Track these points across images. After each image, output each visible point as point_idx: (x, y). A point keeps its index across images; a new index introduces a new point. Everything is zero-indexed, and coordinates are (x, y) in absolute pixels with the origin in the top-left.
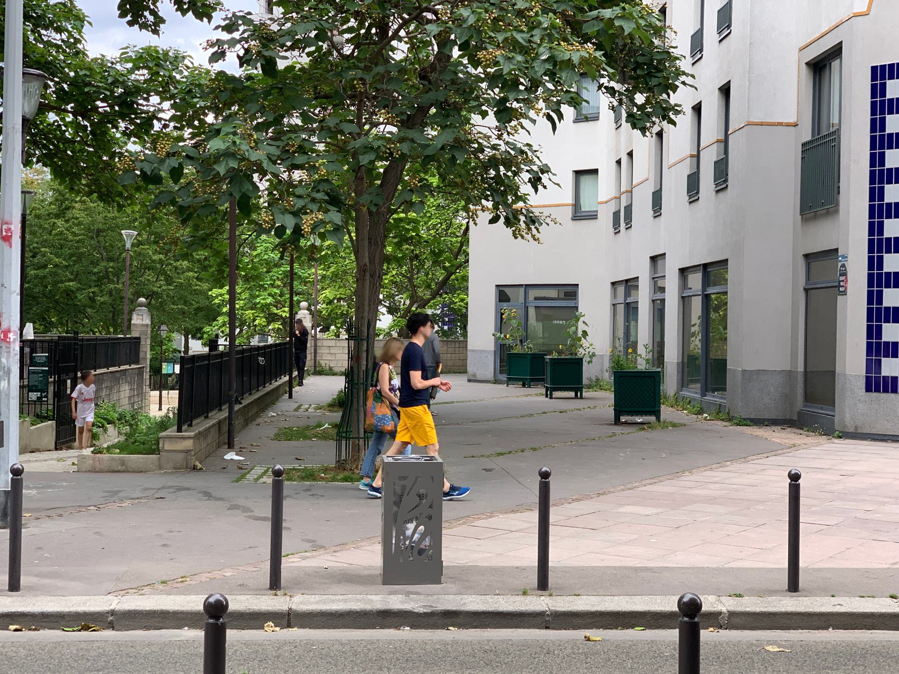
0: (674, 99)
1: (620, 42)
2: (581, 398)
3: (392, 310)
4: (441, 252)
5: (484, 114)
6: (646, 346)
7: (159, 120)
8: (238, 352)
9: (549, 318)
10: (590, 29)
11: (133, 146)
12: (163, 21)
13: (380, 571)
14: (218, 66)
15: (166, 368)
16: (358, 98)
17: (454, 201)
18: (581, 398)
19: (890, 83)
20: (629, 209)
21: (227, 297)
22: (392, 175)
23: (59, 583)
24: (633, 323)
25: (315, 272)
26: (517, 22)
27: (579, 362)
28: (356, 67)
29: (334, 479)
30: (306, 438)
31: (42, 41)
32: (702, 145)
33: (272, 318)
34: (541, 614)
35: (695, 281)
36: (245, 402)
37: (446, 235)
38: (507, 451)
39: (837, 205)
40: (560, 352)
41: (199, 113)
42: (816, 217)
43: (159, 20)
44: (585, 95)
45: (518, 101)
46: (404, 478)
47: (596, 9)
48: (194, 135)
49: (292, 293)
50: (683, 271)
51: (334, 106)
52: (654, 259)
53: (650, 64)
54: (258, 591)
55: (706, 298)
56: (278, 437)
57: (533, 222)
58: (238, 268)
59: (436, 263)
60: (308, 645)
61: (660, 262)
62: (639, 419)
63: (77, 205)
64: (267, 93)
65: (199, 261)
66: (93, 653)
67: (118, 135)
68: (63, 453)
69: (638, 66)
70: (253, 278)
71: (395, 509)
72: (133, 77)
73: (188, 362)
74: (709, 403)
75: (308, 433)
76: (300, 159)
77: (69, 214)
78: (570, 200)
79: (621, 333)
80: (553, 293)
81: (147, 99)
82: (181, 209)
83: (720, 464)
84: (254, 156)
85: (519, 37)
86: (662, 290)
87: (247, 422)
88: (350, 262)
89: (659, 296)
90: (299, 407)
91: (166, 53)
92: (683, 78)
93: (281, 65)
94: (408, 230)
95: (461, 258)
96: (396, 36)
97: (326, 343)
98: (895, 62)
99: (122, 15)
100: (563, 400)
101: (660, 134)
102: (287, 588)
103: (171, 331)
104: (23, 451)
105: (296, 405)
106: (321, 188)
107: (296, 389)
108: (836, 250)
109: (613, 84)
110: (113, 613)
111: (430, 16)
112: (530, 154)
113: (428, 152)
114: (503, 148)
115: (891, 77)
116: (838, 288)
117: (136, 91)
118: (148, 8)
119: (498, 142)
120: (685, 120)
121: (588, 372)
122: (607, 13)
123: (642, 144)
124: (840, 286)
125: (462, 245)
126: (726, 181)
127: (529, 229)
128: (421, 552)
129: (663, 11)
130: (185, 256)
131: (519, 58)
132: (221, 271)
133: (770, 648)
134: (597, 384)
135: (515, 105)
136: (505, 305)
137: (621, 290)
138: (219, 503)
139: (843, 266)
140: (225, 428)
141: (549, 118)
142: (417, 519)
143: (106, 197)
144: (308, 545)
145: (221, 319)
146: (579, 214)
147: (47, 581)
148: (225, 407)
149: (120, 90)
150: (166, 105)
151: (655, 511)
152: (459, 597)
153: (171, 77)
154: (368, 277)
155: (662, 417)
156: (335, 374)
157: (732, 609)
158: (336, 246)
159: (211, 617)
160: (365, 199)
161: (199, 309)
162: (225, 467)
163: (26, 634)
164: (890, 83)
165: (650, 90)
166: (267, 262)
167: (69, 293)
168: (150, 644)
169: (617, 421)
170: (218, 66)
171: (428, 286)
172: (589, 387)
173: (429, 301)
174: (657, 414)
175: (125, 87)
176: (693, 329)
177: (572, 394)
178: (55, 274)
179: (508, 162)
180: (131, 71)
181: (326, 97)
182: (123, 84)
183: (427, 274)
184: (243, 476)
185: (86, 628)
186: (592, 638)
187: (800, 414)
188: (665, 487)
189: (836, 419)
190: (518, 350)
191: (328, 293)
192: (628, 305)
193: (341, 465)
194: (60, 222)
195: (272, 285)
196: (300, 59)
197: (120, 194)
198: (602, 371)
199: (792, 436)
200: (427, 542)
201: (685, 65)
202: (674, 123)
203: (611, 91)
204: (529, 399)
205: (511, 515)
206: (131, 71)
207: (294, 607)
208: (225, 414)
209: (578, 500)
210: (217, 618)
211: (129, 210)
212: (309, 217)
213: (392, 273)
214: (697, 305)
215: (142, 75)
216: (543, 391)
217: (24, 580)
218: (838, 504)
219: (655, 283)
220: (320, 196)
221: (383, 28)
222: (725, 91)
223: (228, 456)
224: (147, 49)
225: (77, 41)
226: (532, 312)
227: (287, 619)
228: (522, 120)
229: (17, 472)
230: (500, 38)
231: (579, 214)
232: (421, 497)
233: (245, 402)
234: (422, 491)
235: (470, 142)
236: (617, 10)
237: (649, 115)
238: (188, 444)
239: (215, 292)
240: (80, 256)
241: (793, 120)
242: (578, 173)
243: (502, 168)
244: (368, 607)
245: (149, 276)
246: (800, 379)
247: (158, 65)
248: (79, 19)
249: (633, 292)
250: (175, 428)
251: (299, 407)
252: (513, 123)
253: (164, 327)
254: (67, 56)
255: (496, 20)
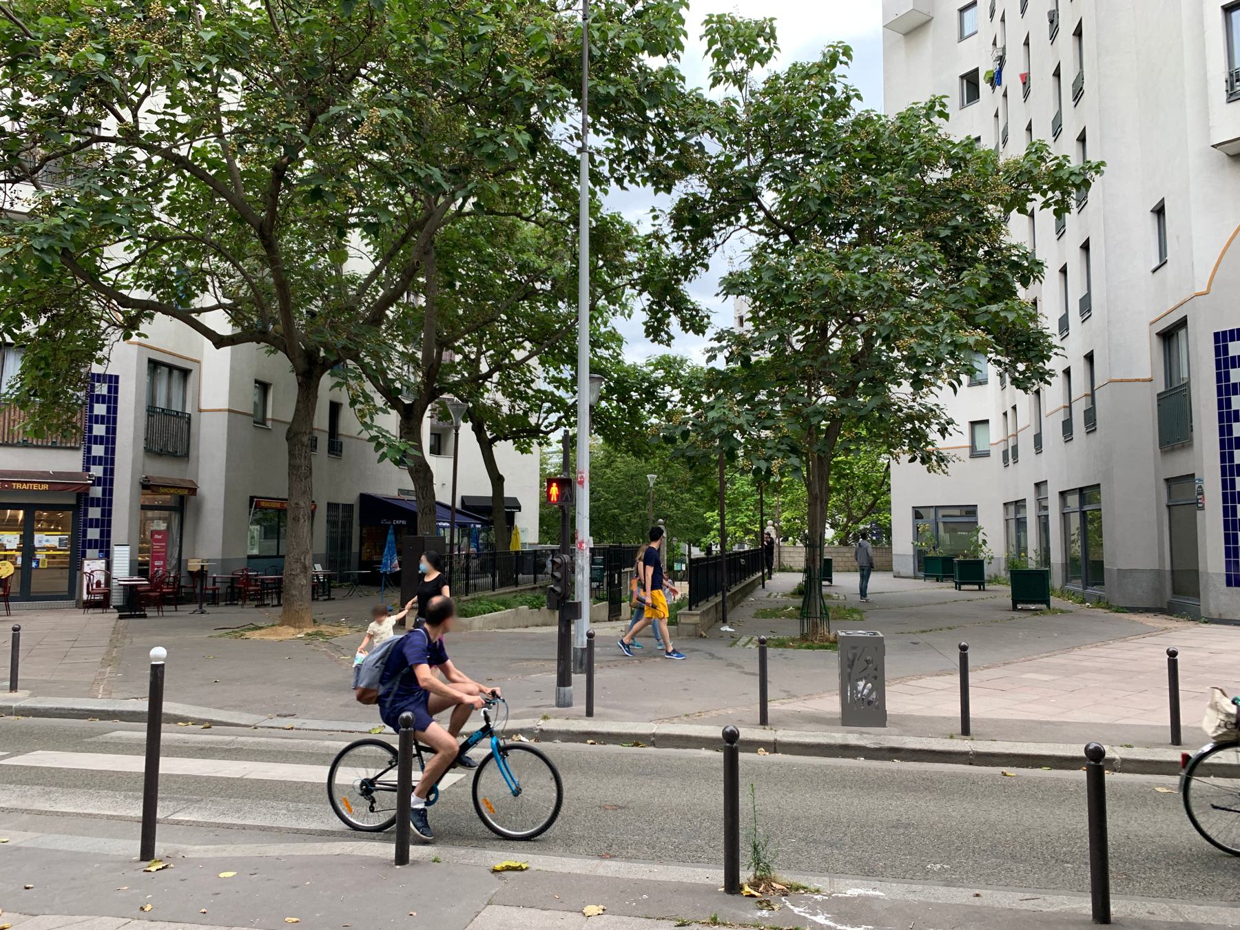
0: (1048, 366)
1: (1004, 327)
2: (984, 590)
3: (833, 526)
4: (870, 484)
5: (899, 384)
6: (1035, 552)
7: (671, 402)
8: (727, 556)
9: (954, 530)
10: (981, 320)
11: (654, 420)
12: (673, 338)
13: (839, 716)
14: (713, 364)
15: (677, 567)
16: (809, 379)
17: (878, 447)
18: (984, 590)
19: (1231, 345)
20: (1015, 448)
21: (717, 518)
22: (832, 432)
23: (618, 712)
24: (1022, 534)
25: (775, 500)
26: (925, 319)
27: (981, 563)
28: (806, 358)
29: (800, 647)
30: (777, 617)
31: (597, 356)
32: (1073, 399)
33: (748, 532)
34: (966, 753)
35: (1073, 501)
36: (733, 591)
37: (872, 472)
38: (928, 629)
39: (1191, 439)
40: (965, 556)
41: (697, 396)
42: (1173, 450)
43: (671, 338)
44: (976, 365)
45: (928, 374)
46: (855, 648)
47: (984, 305)
48: (694, 411)
49: (762, 515)
50: (1063, 494)
51: (789, 385)
52: (1037, 485)
53: (1028, 342)
54: (751, 725)
55: (1083, 514)
56: (756, 616)
57: (943, 461)
58: (725, 498)
59: (866, 492)
60: (790, 766)
61: (1043, 487)
62: (1033, 607)
63: (619, 460)
64: (745, 380)
65: (697, 493)
66: (642, 763)
67: (645, 413)
68: (614, 624)
69: (1018, 343)
70: (734, 505)
71: (849, 670)
72: (654, 375)
73: (694, 563)
74: (1091, 595)
75: (777, 613)
76: (769, 423)
77: (614, 466)
78: (967, 442)
79: (1013, 541)
80: (957, 512)
81: (663, 389)
82: (690, 459)
83: (1104, 642)
84: (738, 422)
85: (927, 329)
86: (1046, 508)
87: (734, 605)
88: (802, 491)
89: (1044, 513)
90: (770, 595)
91: (675, 359)
92: (1055, 350)
93: (754, 359)
94: (845, 469)
95: (885, 488)
96: (834, 335)
97: (786, 549)
98: (1235, 327)
99: (648, 336)
100: (969, 592)
101: (1038, 392)
102: (771, 725)
103: (679, 541)
104: (593, 621)
105: (768, 593)
106: (784, 441)
107: (767, 581)
108: (1193, 475)
109: (999, 357)
110: (654, 735)
111: (858, 319)
112: (938, 411)
113: (862, 413)
114: (917, 407)
115: (1232, 340)
116: (1196, 504)
117: (656, 384)
118: (663, 330)
119: (912, 404)
120: (1058, 381)
121: (988, 570)
122: (994, 308)
123: (1024, 400)
124: (1198, 503)
125: (885, 478)
126: (1095, 424)
127: (940, 466)
128: (870, 703)
129: (1035, 303)
130: (688, 491)
131: (928, 344)
132: (712, 500)
133: (1159, 789)
134: (995, 580)
135: (926, 377)
136: (920, 521)
137: (1012, 508)
138: (720, 661)
139: (1200, 487)
140: (720, 609)
141: (951, 385)
142: (865, 678)
143: (638, 454)
144: (784, 695)
145: (712, 533)
146: (975, 453)
147: (610, 711)
148: (720, 594)
149: (646, 384)
150: (676, 392)
151: (1052, 678)
152: (900, 738)
153: (678, 374)
154: (819, 502)
155: (1052, 605)
156: (794, 571)
157: (1124, 756)
158: (791, 481)
159: (728, 742)
160: (815, 448)
161: (697, 527)
162: (722, 636)
163: (598, 747)
164: (1231, 345)
165: (1028, 360)
166: (743, 494)
167: (614, 517)
168: (680, 759)
169: (1015, 608)
170: (713, 364)
171: (861, 508)
172: (990, 582)
173: (861, 519)
174: (1047, 603)
175: (649, 382)
176: (1073, 538)
177: (976, 587)
178: (606, 504)
179: (921, 418)
180: (653, 372)
181: (784, 379)
182: (648, 380)
183: (859, 500)
184: (735, 643)
185: (637, 745)
186: (1008, 774)
187: (1170, 603)
188: (1059, 660)
189: (1202, 608)
190: (932, 554)
191: (786, 515)
192: (1018, 520)
193: (804, 638)
194: (608, 471)
195: (747, 509)
196: (765, 355)
197: (647, 452)
198: (999, 570)
199: (1164, 621)
200: (874, 696)
201: (1055, 340)
202: (1049, 384)
203: (998, 363)
204: (942, 590)
205: (936, 678)
206: (653, 372)
207: (778, 739)
208: (719, 599)
209: (988, 668)
210: (732, 743)
211: (652, 461)
212: (776, 462)
213: (834, 499)
214: (1075, 520)
215: (660, 373)
216: (954, 585)
217: (596, 709)
218: (1209, 676)
219: (1040, 503)
220: (783, 447)
221: (824, 329)
222: (1090, 358)
223: (723, 629)
224: (663, 357)
225: (619, 355)
226: (941, 526)
227: (774, 747)
228: (932, 388)
229: (590, 636)
230: (913, 330)
231: (975, 453)
232: (868, 662)
233: (733, 591)
234: (868, 658)
235: (894, 404)
236: (1002, 305)
237: (1029, 379)
238: (696, 619)
239: (708, 514)
240: (621, 492)
241: (1148, 376)
242: (973, 424)
243: (916, 422)
244: (832, 742)
245: (665, 504)
246: (1168, 576)
247: (670, 366)
248: (620, 341)
249: (1022, 510)
250: (687, 608)
251: (770, 595)
252: (925, 390)
253: (675, 539)
254: (612, 364)
255: (909, 319)
